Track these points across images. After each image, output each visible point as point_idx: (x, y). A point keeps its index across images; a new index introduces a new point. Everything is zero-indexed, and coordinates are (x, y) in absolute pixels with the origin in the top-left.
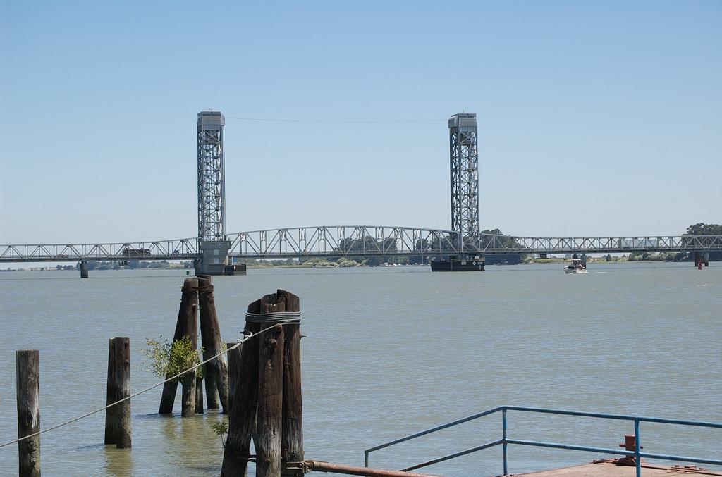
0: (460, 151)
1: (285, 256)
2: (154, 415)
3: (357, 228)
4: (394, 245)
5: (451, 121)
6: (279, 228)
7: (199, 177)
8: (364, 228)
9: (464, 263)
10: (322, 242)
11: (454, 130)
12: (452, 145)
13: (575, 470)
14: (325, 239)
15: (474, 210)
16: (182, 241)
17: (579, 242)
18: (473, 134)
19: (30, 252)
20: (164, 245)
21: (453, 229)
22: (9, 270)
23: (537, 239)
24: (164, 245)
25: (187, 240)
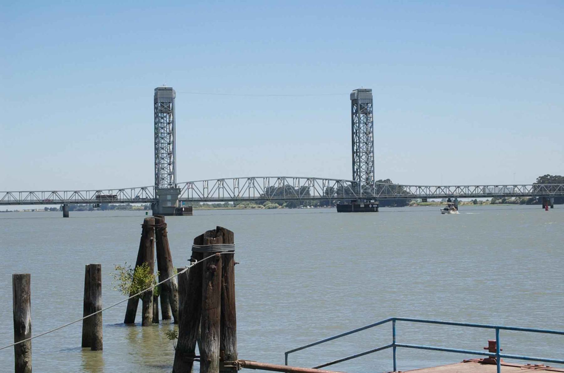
0: (359, 118)
1: (222, 201)
4: (308, 192)
5: (352, 95)
8: (284, 178)
9: (362, 206)
10: (252, 189)
11: (354, 102)
12: (353, 114)
14: (224, 187)
16: (142, 188)
18: (370, 105)
23: (420, 187)
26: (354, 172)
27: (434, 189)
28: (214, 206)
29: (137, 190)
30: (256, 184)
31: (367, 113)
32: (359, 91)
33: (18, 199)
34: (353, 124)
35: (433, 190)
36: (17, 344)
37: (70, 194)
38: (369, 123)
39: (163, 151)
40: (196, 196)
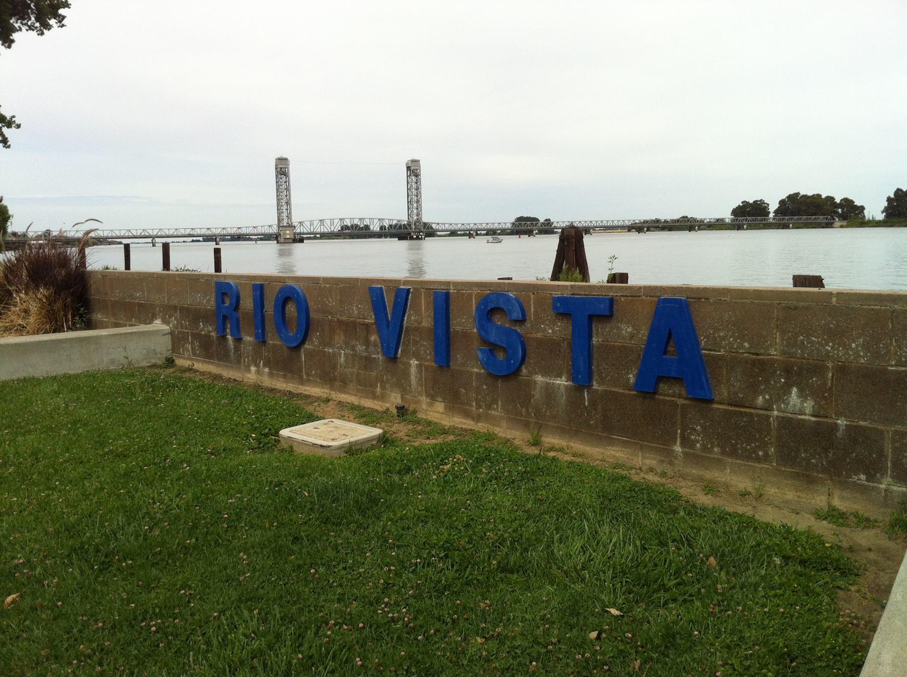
0: (412, 179)
1: (312, 234)
2: (587, 230)
3: (379, 220)
4: (369, 229)
5: (407, 164)
6: (379, 218)
7: (277, 192)
8: (383, 219)
9: (415, 237)
10: (322, 227)
11: (408, 168)
12: (407, 176)
13: (474, 306)
14: (323, 225)
15: (419, 209)
16: (269, 226)
17: (472, 226)
18: (418, 171)
19: (171, 232)
20: (229, 230)
21: (409, 219)
22: (184, 242)
23: (451, 224)
24: (560, 223)
25: (272, 225)
26: (409, 215)
27: (577, 223)
28: (193, 241)
29: (266, 227)
30: (325, 224)
31: (417, 175)
32: (413, 161)
33: (102, 235)
34: (408, 183)
35: (459, 226)
36: (799, 293)
37: (219, 230)
38: (287, 182)
39: (282, 201)
40: (305, 231)
